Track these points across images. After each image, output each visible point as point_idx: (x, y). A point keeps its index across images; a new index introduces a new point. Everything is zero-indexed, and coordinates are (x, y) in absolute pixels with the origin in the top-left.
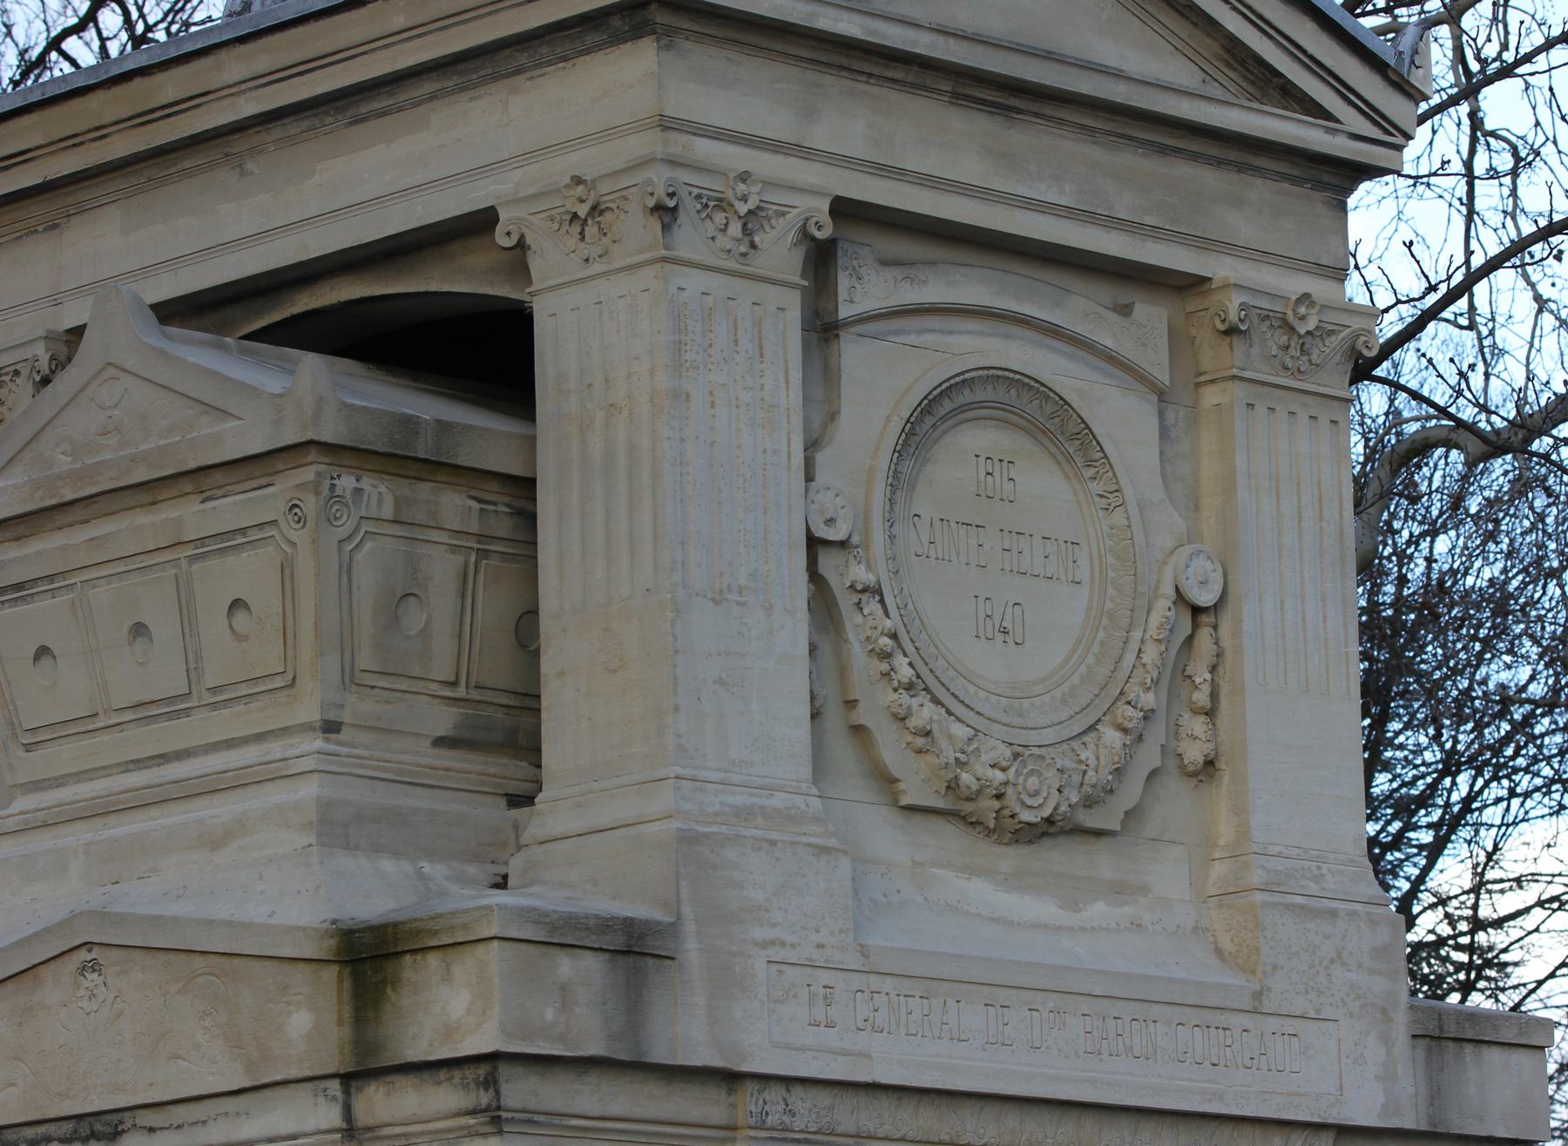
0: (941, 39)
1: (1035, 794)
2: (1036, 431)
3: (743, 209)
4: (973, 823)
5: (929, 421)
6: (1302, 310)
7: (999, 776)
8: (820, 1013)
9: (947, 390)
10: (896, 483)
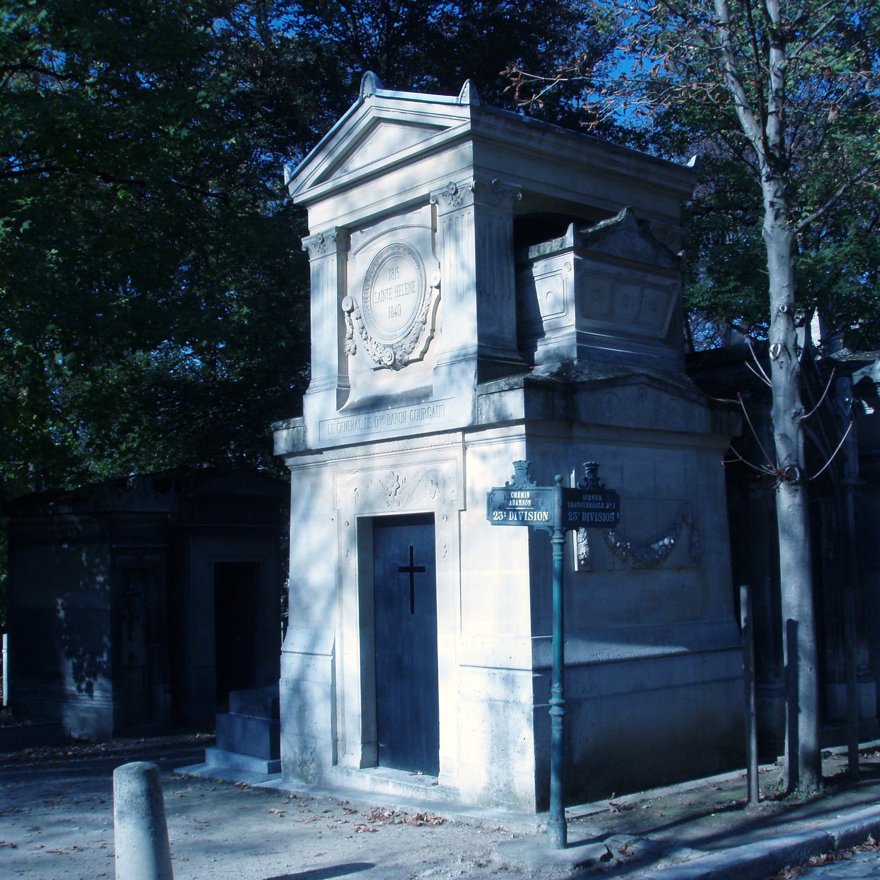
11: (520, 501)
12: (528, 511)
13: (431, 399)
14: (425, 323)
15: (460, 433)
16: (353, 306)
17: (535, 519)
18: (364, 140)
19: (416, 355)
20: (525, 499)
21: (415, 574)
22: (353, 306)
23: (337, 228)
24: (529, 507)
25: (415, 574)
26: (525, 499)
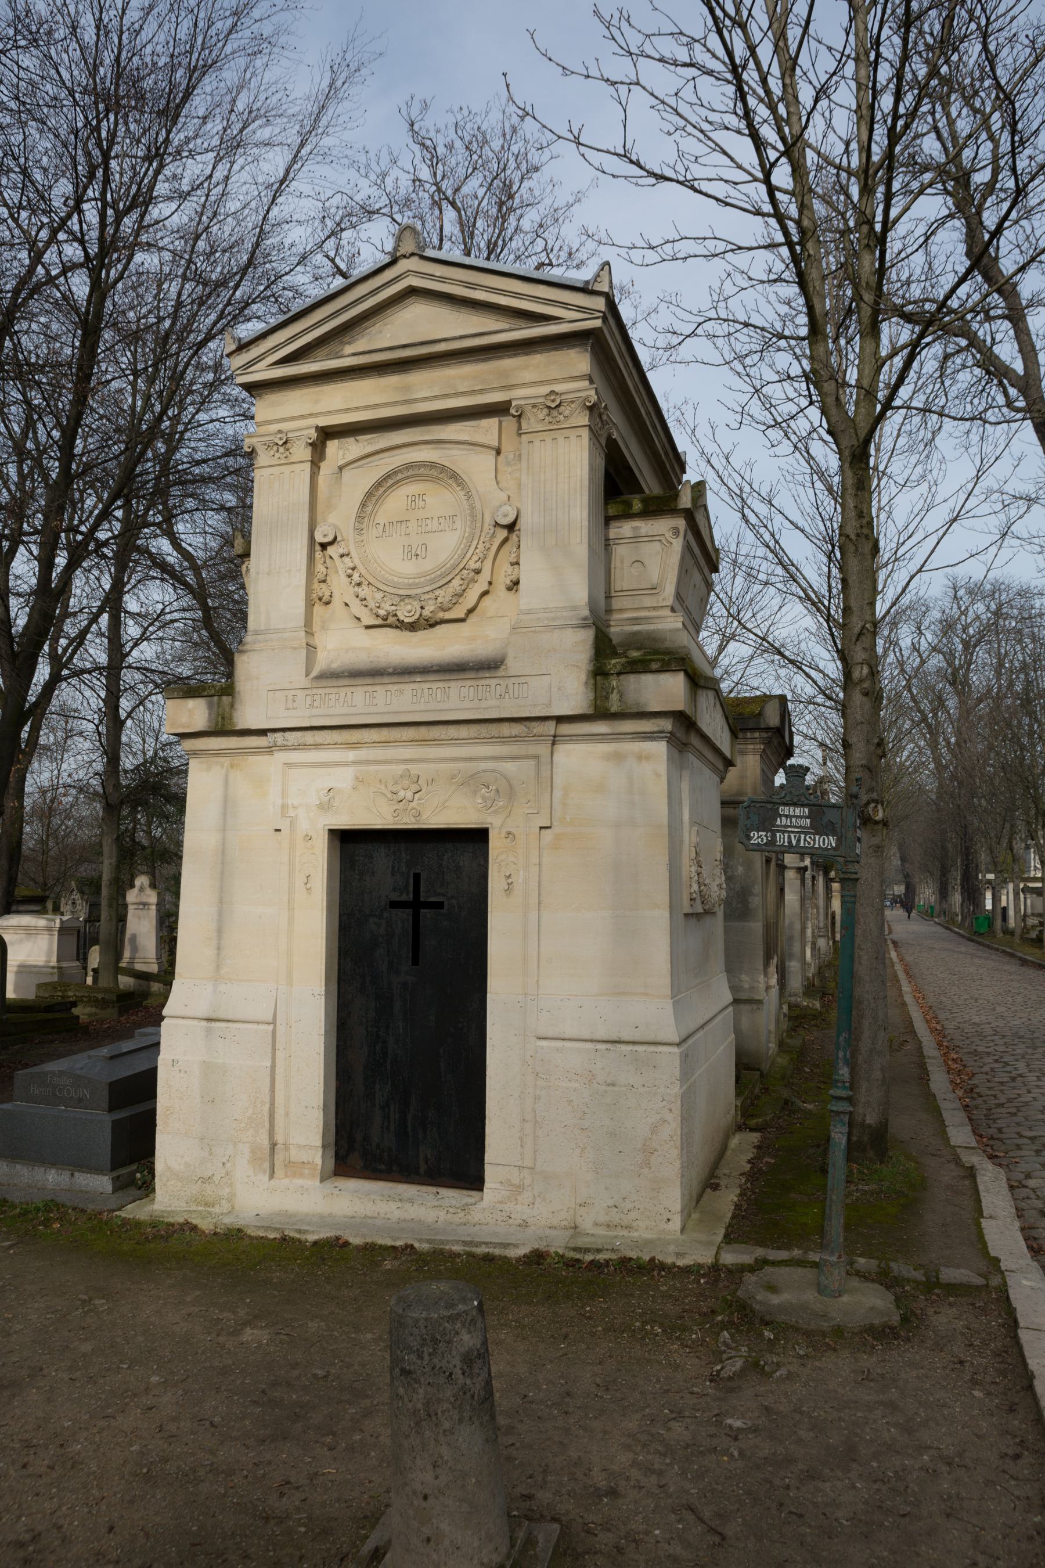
0: (356, 358)
1: (409, 612)
2: (434, 479)
3: (280, 443)
4: (390, 626)
5: (381, 490)
6: (552, 397)
7: (393, 608)
8: (290, 705)
9: (388, 477)
10: (360, 518)
11: (794, 820)
12: (806, 834)
13: (501, 672)
14: (478, 572)
15: (552, 724)
16: (336, 538)
17: (817, 846)
18: (467, 306)
19: (459, 612)
20: (801, 817)
21: (410, 911)
22: (336, 538)
23: (317, 427)
24: (195, 753)
25: (410, 911)
26: (801, 817)
